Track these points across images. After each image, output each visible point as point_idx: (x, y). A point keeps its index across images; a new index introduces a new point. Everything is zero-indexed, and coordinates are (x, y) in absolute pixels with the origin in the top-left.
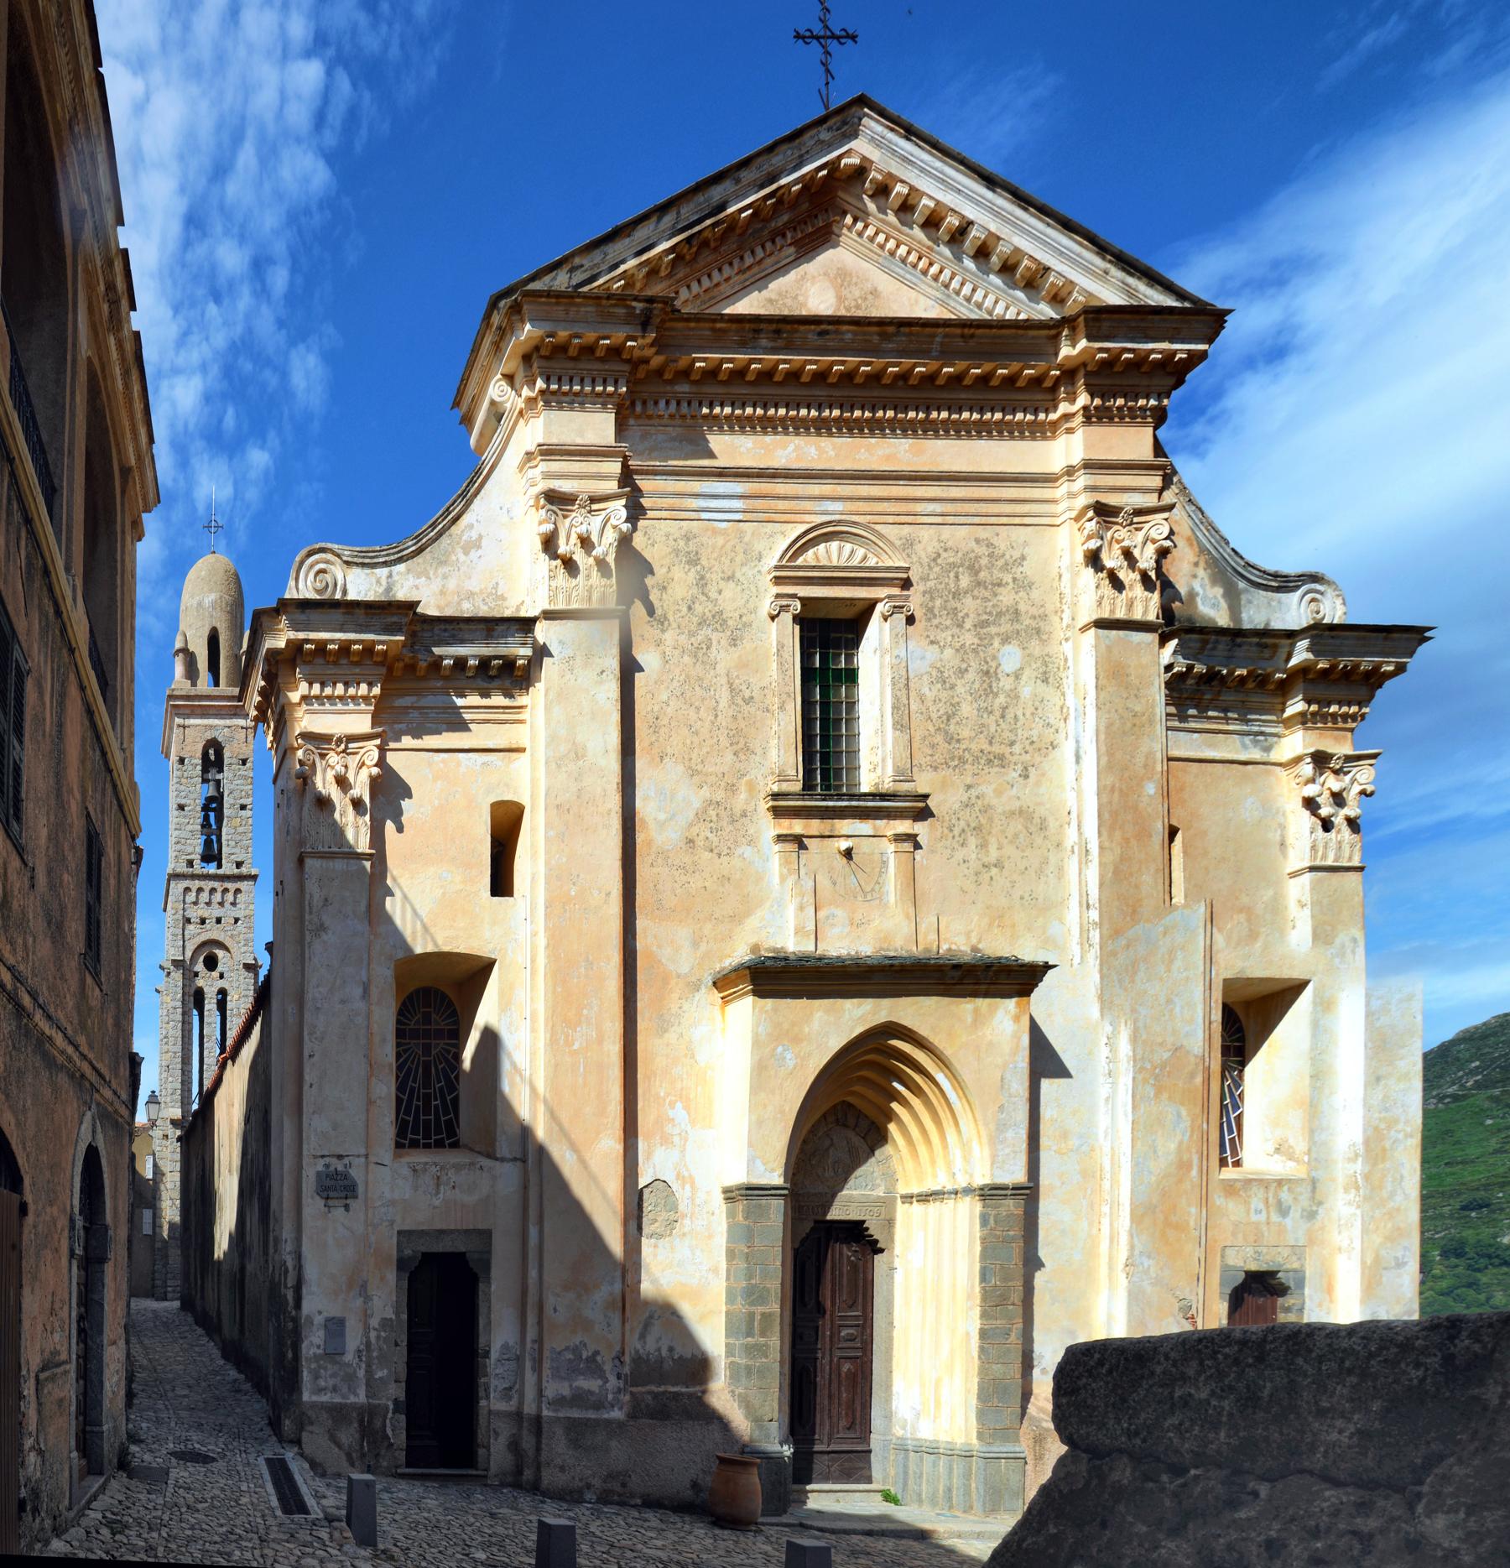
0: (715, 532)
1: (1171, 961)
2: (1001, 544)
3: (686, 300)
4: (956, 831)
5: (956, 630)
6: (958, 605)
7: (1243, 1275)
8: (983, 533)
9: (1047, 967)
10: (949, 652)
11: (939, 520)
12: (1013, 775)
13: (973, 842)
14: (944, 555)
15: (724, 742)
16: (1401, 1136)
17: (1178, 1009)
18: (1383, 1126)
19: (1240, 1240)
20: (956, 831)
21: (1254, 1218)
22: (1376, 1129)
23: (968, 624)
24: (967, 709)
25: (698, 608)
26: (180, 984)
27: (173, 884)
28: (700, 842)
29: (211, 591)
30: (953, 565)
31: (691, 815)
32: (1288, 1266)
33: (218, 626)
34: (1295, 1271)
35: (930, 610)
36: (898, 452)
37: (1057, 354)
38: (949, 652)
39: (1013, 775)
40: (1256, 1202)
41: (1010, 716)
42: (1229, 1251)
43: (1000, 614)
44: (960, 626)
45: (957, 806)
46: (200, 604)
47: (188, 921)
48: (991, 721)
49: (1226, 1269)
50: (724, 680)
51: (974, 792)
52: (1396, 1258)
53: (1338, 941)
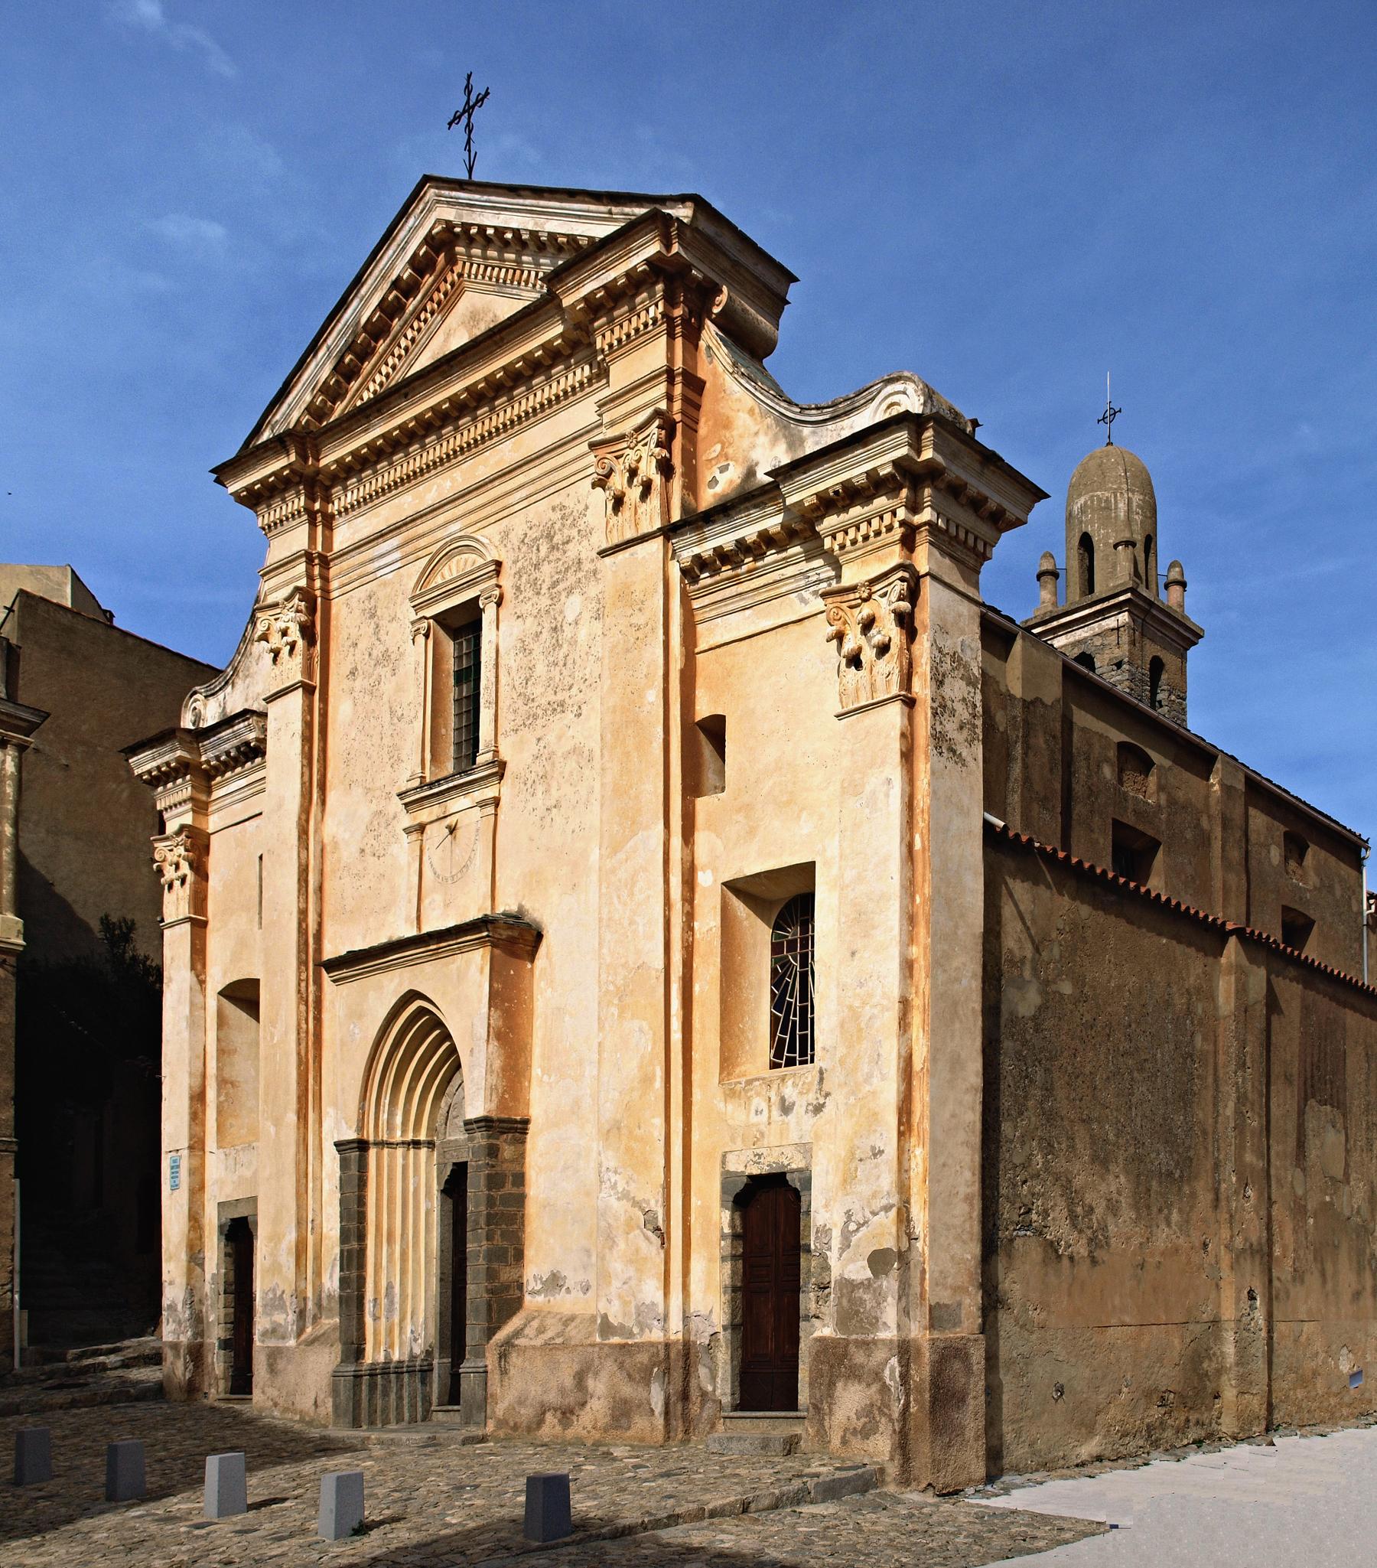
0: (385, 584)
1: (634, 884)
2: (570, 503)
3: (317, 489)
4: (529, 783)
5: (535, 599)
6: (538, 575)
7: (745, 1180)
8: (556, 500)
9: (257, 1019)
10: (530, 620)
11: (525, 503)
12: (570, 716)
13: (540, 789)
14: (530, 533)
15: (386, 758)
16: (876, 1011)
17: (641, 928)
18: (857, 1004)
19: (739, 1145)
20: (529, 783)
21: (754, 1119)
22: (851, 1008)
23: (545, 587)
24: (541, 669)
25: (375, 653)
28: (368, 851)
30: (536, 539)
31: (364, 827)
32: (794, 1166)
34: (800, 1170)
35: (518, 588)
36: (506, 452)
37: (88, 929)
38: (530, 620)
39: (570, 716)
40: (758, 1102)
41: (570, 662)
42: (729, 1157)
43: (567, 570)
44: (538, 593)
45: (530, 761)
48: (555, 672)
49: (727, 1177)
50: (387, 707)
51: (542, 744)
52: (873, 1148)
53: (868, 788)
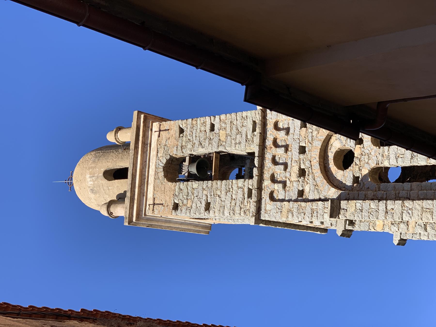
26: (359, 203)
27: (262, 218)
29: (85, 179)
33: (103, 170)
46: (92, 191)
47: (301, 193)
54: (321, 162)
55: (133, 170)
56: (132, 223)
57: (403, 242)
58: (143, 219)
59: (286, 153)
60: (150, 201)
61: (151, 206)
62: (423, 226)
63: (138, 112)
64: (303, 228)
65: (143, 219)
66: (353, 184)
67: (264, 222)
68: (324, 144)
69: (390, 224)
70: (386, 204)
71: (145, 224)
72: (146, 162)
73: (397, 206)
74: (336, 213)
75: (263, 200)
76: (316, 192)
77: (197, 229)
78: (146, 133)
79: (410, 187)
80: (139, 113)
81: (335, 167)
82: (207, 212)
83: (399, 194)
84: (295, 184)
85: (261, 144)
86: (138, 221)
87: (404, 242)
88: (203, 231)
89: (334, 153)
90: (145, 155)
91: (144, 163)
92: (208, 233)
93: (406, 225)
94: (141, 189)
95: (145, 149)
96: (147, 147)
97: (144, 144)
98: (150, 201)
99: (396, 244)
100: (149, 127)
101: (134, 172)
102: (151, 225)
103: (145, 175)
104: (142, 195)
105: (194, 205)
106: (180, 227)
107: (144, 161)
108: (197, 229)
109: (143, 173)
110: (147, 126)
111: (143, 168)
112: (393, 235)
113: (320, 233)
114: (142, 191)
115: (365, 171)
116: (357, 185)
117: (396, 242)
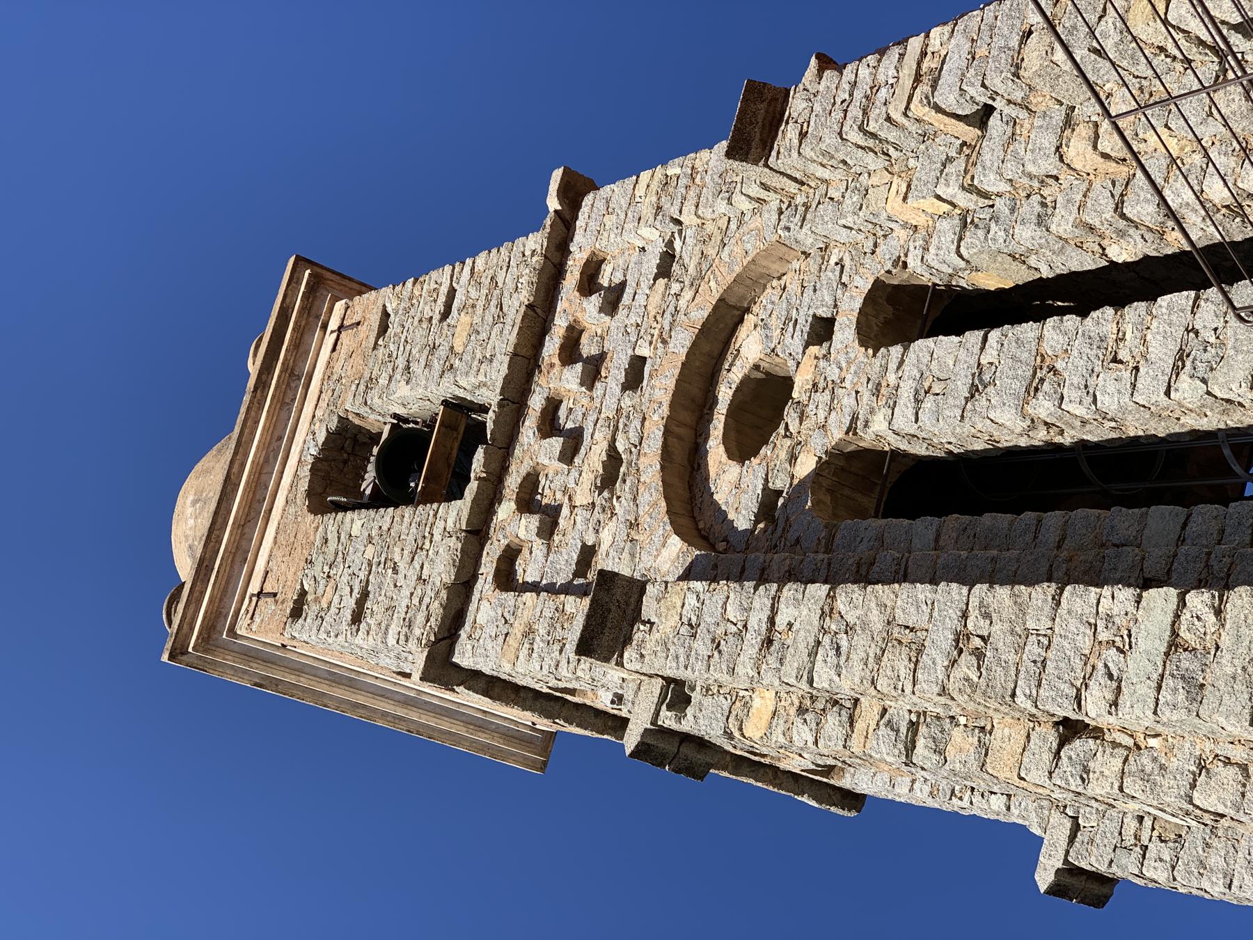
54: (681, 424)
55: (232, 462)
56: (184, 658)
57: (1084, 886)
58: (226, 648)
59: (591, 387)
60: (254, 588)
61: (255, 599)
62: (903, 730)
63: (298, 259)
64: (599, 722)
65: (226, 648)
66: (757, 522)
67: (482, 684)
68: (706, 348)
69: (793, 711)
70: (776, 600)
71: (245, 671)
72: (280, 438)
73: (805, 612)
74: (616, 639)
75: (479, 586)
76: (626, 555)
77: (483, 738)
78: (306, 337)
79: (932, 537)
80: (301, 262)
81: (722, 448)
82: (354, 628)
83: (872, 564)
84: (581, 515)
85: (523, 352)
86: (206, 651)
87: (1096, 889)
88: (514, 754)
89: (734, 386)
90: (284, 414)
91: (275, 444)
92: (541, 769)
93: (845, 718)
94: (242, 534)
95: (290, 394)
96: (297, 387)
97: (292, 374)
98: (254, 588)
99: (1043, 888)
100: (318, 317)
101: (235, 470)
102: (276, 683)
103: (267, 488)
104: (239, 558)
105: (336, 599)
106: (400, 712)
107: (276, 434)
108: (483, 738)
109: (263, 477)
110: (313, 312)
111: (266, 461)
112: (1040, 840)
113: (816, 805)
114: (243, 543)
115: (806, 465)
116: (764, 530)
117: (1044, 878)
